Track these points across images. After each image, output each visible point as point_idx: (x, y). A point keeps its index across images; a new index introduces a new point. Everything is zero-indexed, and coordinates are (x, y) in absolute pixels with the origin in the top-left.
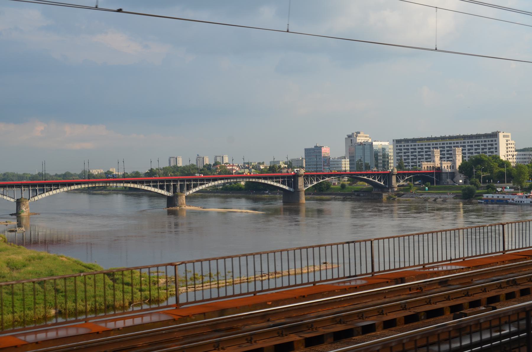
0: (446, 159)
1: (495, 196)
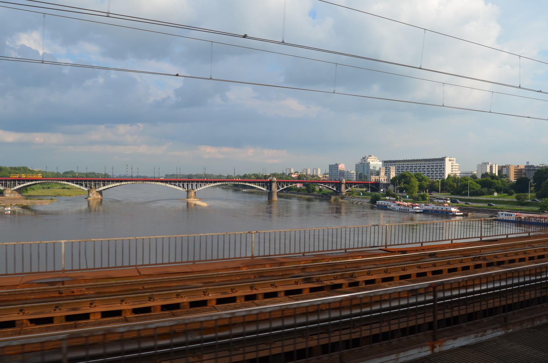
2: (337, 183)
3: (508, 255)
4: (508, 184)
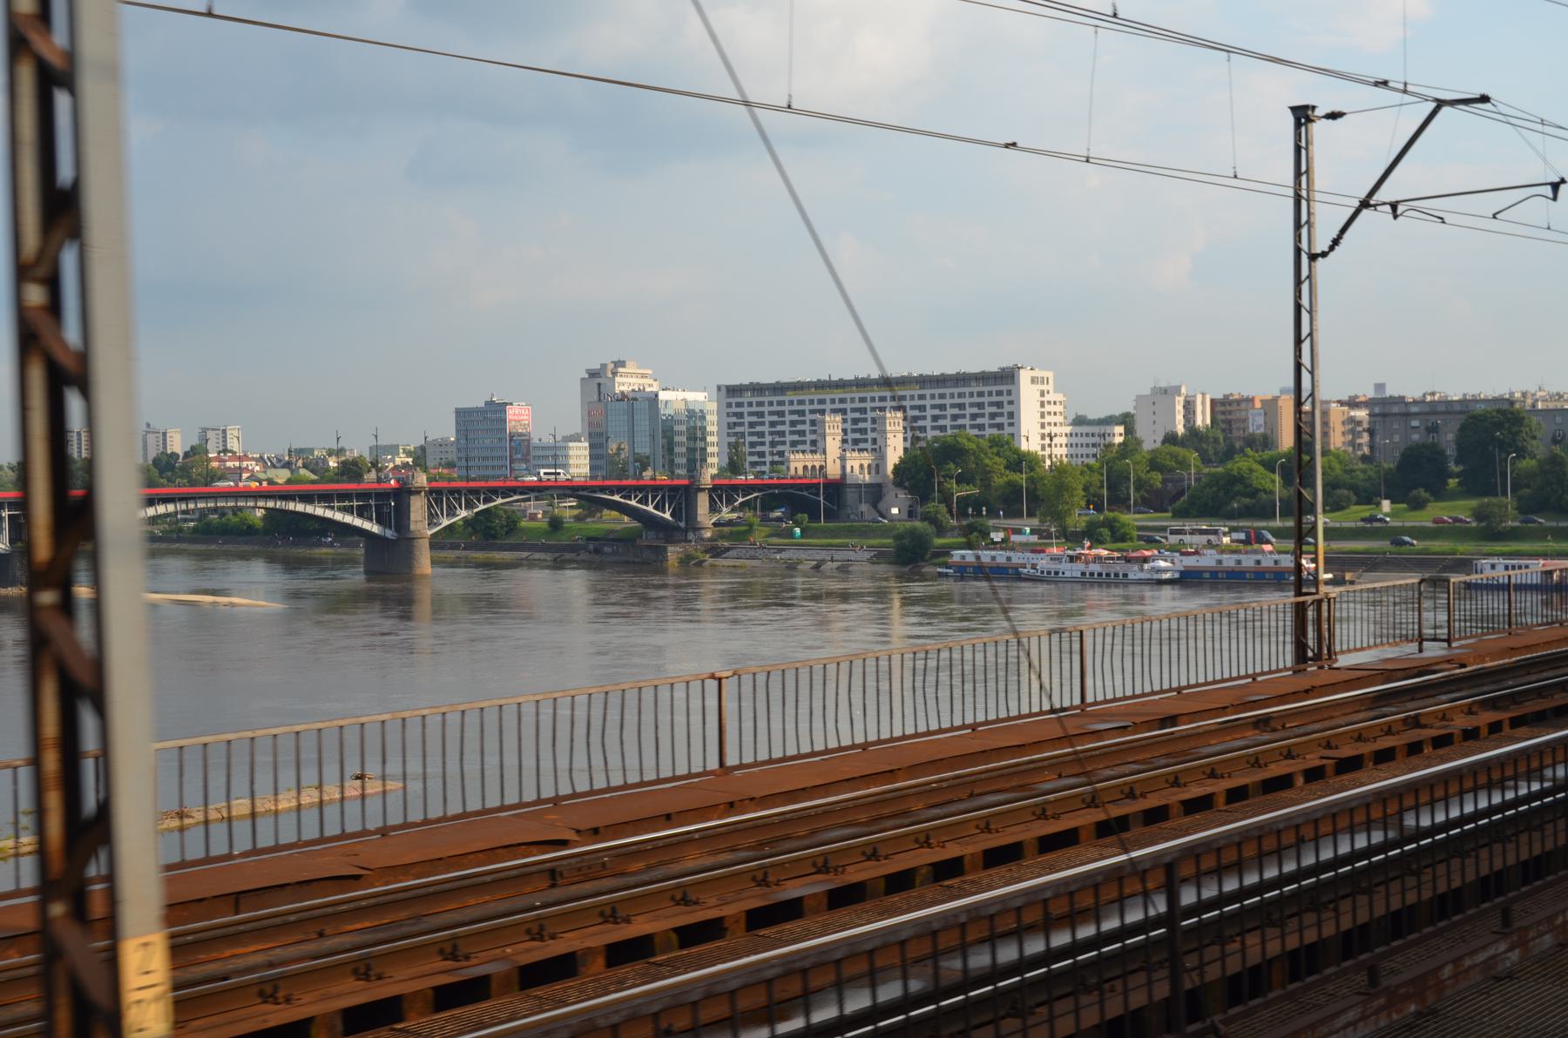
0: (807, 447)
1: (986, 556)
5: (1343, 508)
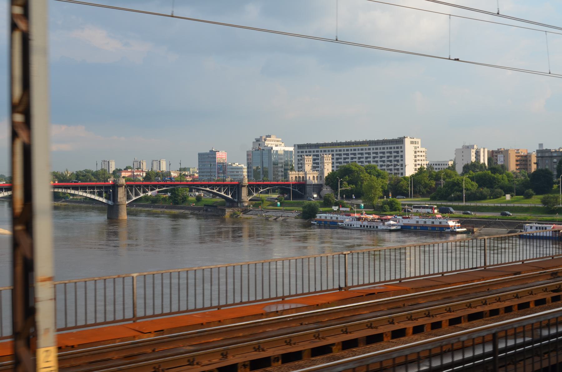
2: (232, 186)
3: (452, 310)
4: (518, 181)
5: (498, 197)
